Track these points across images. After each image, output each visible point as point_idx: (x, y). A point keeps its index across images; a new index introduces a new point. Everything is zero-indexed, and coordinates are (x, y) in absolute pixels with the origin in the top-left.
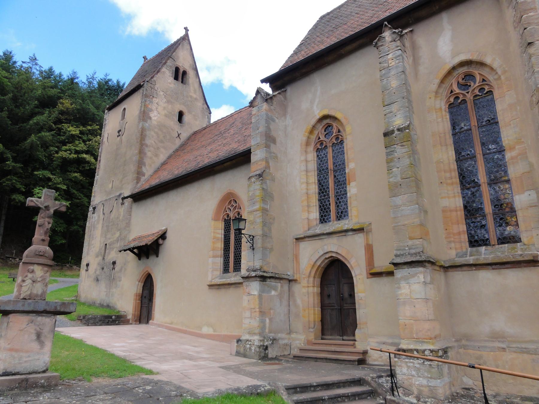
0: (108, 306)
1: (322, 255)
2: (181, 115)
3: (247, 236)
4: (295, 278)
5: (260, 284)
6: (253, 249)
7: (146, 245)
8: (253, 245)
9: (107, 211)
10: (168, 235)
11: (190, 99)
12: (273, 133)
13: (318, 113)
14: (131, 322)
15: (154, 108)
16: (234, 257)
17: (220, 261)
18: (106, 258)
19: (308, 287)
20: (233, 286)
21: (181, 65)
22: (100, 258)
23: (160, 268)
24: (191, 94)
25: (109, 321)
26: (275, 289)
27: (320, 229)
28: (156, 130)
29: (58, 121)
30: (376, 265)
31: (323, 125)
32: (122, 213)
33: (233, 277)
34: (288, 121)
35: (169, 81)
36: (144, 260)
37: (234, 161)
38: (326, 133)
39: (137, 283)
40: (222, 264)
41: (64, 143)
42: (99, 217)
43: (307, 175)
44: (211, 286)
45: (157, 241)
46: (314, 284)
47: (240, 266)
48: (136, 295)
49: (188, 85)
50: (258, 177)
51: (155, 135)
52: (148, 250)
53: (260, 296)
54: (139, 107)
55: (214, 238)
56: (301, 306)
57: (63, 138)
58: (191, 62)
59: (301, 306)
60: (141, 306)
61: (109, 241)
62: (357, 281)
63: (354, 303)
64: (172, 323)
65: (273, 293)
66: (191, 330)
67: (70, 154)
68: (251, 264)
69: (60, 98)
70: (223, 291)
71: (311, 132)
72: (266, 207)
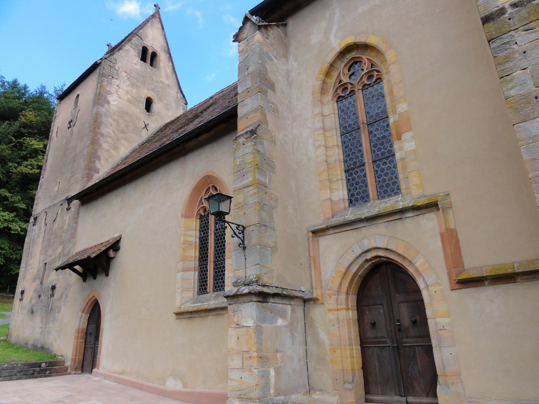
0: (43, 348)
1: (360, 255)
2: (149, 103)
3: (234, 227)
4: (315, 296)
5: (257, 306)
6: (244, 248)
7: (89, 257)
8: (243, 242)
9: (49, 220)
10: (122, 244)
11: (160, 84)
12: (271, 76)
13: (338, 45)
14: (69, 371)
15: (113, 90)
16: (215, 269)
17: (193, 276)
18: (44, 282)
19: (338, 310)
20: (213, 313)
21: (149, 45)
22: (38, 282)
23: (112, 293)
24: (162, 79)
25: (34, 371)
26: (283, 315)
27: (350, 215)
28: (116, 117)
29: (19, 135)
30: (467, 265)
31: (346, 61)
32: (67, 222)
33: (213, 300)
34: (293, 64)
35: (135, 61)
36: (90, 281)
37: (212, 132)
38: (350, 73)
39: (80, 313)
40: (196, 281)
41: (25, 158)
42: (40, 229)
43: (325, 136)
44: (179, 314)
45: (106, 251)
46: (347, 304)
47: (224, 282)
48: (78, 331)
49: (159, 68)
50: (249, 134)
51: (114, 123)
52: (95, 266)
53: (258, 329)
54: (94, 90)
55: (185, 242)
56: (327, 342)
57: (25, 153)
58: (163, 43)
59: (327, 342)
60: (85, 348)
61: (50, 259)
62: (430, 296)
63: (426, 335)
64: (123, 373)
65: (280, 322)
66: (150, 384)
67: (31, 169)
68: (241, 274)
69: (23, 109)
70: (197, 322)
71: (328, 74)
72: (263, 179)
